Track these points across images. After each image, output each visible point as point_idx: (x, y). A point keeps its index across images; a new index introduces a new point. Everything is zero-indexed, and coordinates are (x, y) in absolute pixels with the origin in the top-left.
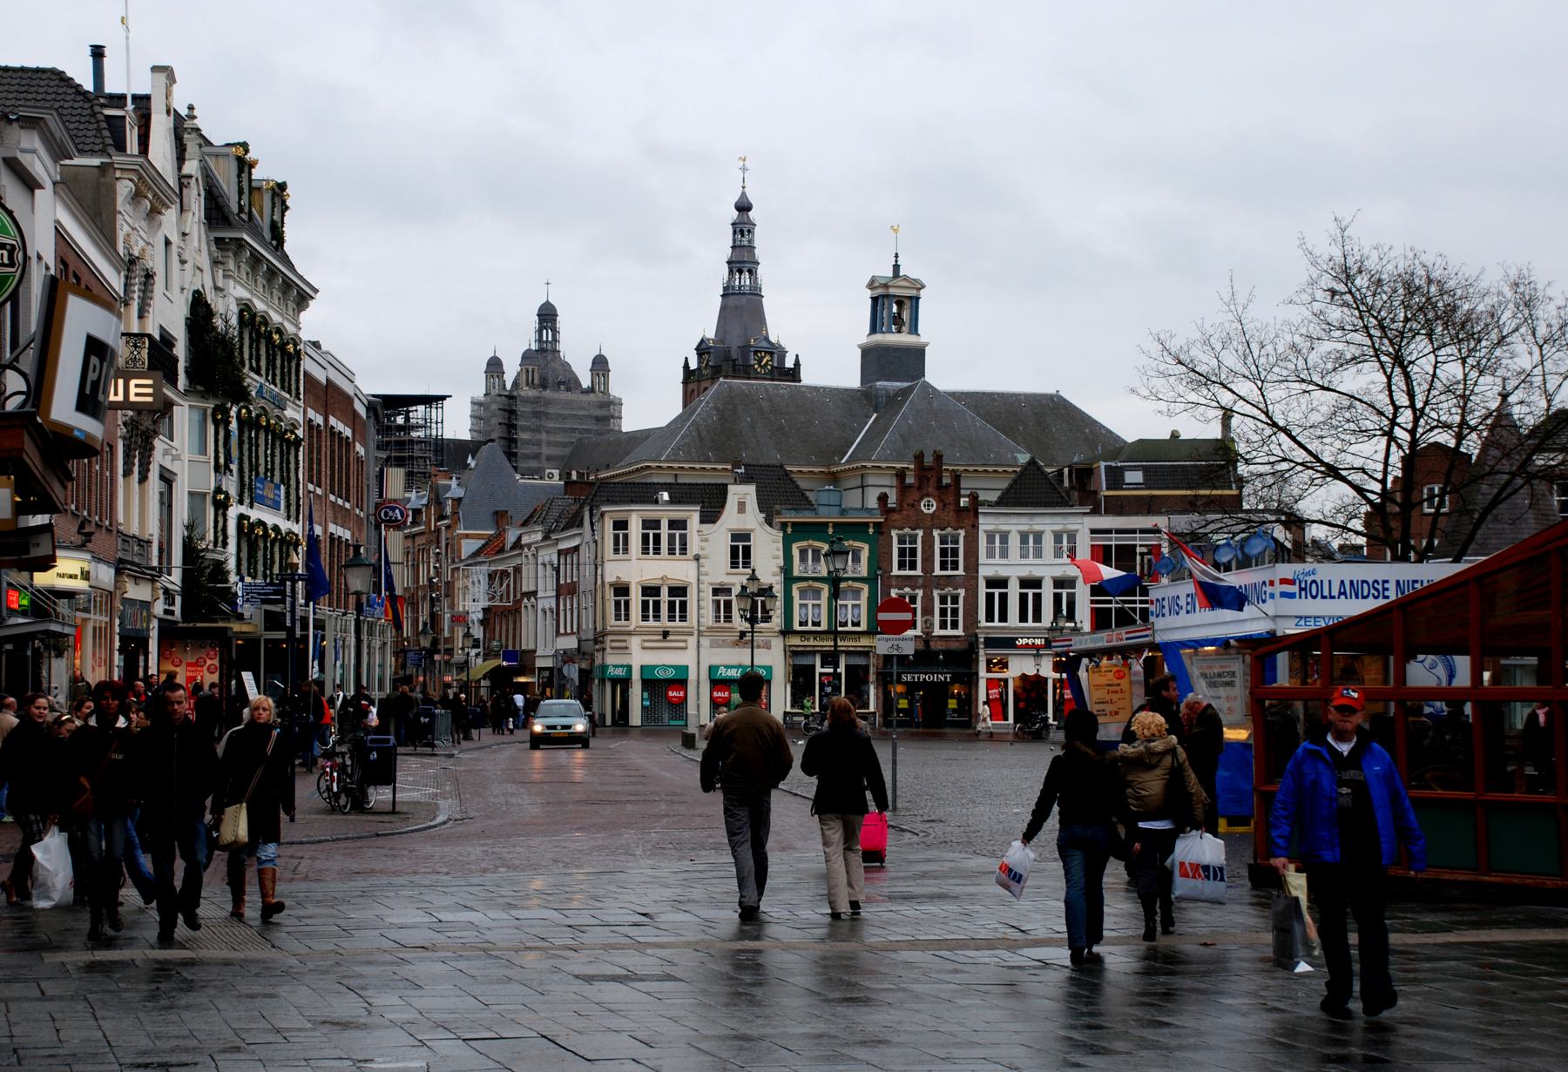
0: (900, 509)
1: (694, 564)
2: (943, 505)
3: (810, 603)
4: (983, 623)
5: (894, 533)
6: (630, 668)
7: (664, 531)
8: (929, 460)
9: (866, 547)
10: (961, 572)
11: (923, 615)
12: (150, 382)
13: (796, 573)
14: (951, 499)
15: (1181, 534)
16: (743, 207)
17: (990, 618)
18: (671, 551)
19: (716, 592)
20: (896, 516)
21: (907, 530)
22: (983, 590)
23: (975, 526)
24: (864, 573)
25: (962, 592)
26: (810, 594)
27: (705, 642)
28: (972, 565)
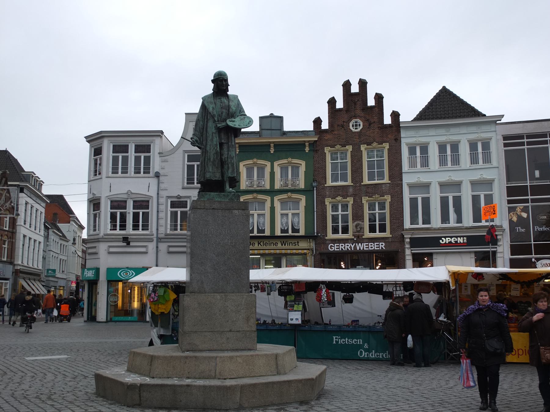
1: (155, 180)
2: (368, 124)
3: (290, 213)
4: (407, 224)
6: (97, 270)
7: (132, 154)
8: (355, 89)
9: (303, 163)
10: (386, 180)
11: (354, 220)
14: (376, 119)
17: (414, 220)
18: (137, 171)
19: (173, 205)
20: (328, 136)
21: (338, 147)
22: (407, 196)
23: (398, 140)
24: (302, 186)
25: (388, 198)
26: (290, 204)
27: (163, 247)
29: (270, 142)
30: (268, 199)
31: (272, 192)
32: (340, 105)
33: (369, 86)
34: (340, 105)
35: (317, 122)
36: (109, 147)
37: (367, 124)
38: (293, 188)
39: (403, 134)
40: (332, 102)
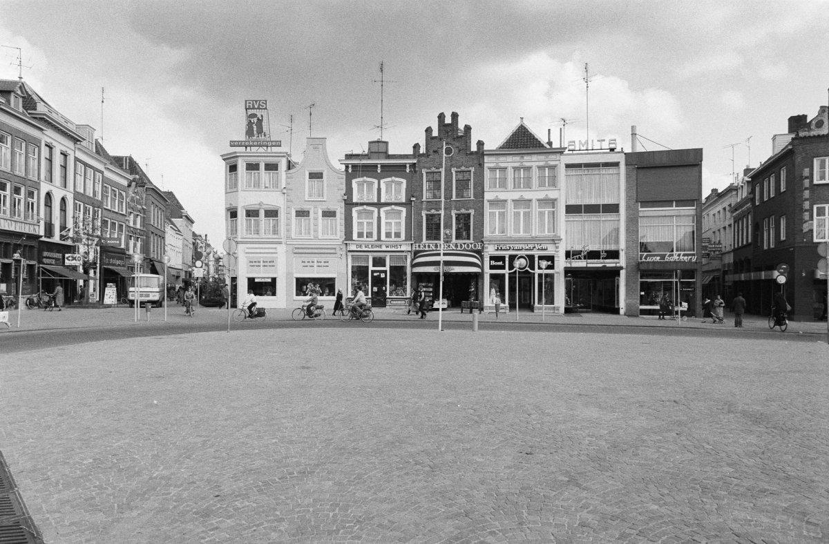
0: (427, 155)
5: (424, 171)
8: (448, 120)
9: (404, 181)
12: (772, 246)
13: (355, 200)
15: (663, 271)
16: (549, 130)
23: (481, 165)
28: (480, 194)
29: (406, 163)
30: (376, 210)
31: (379, 205)
32: (435, 133)
33: (460, 119)
34: (435, 133)
35: (416, 147)
36: (242, 166)
37: (457, 151)
38: (368, 201)
39: (486, 159)
40: (429, 130)
